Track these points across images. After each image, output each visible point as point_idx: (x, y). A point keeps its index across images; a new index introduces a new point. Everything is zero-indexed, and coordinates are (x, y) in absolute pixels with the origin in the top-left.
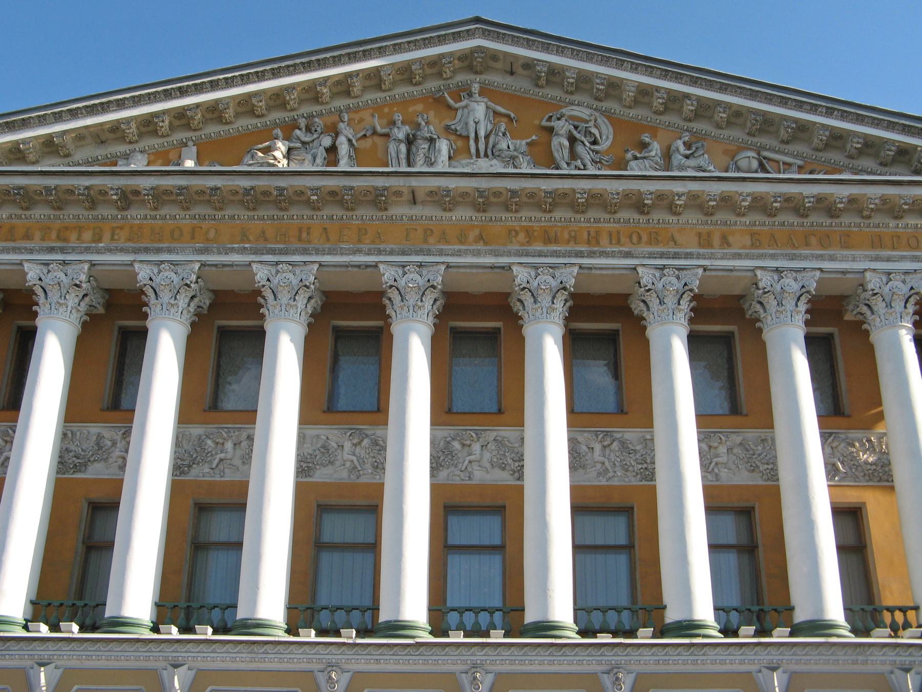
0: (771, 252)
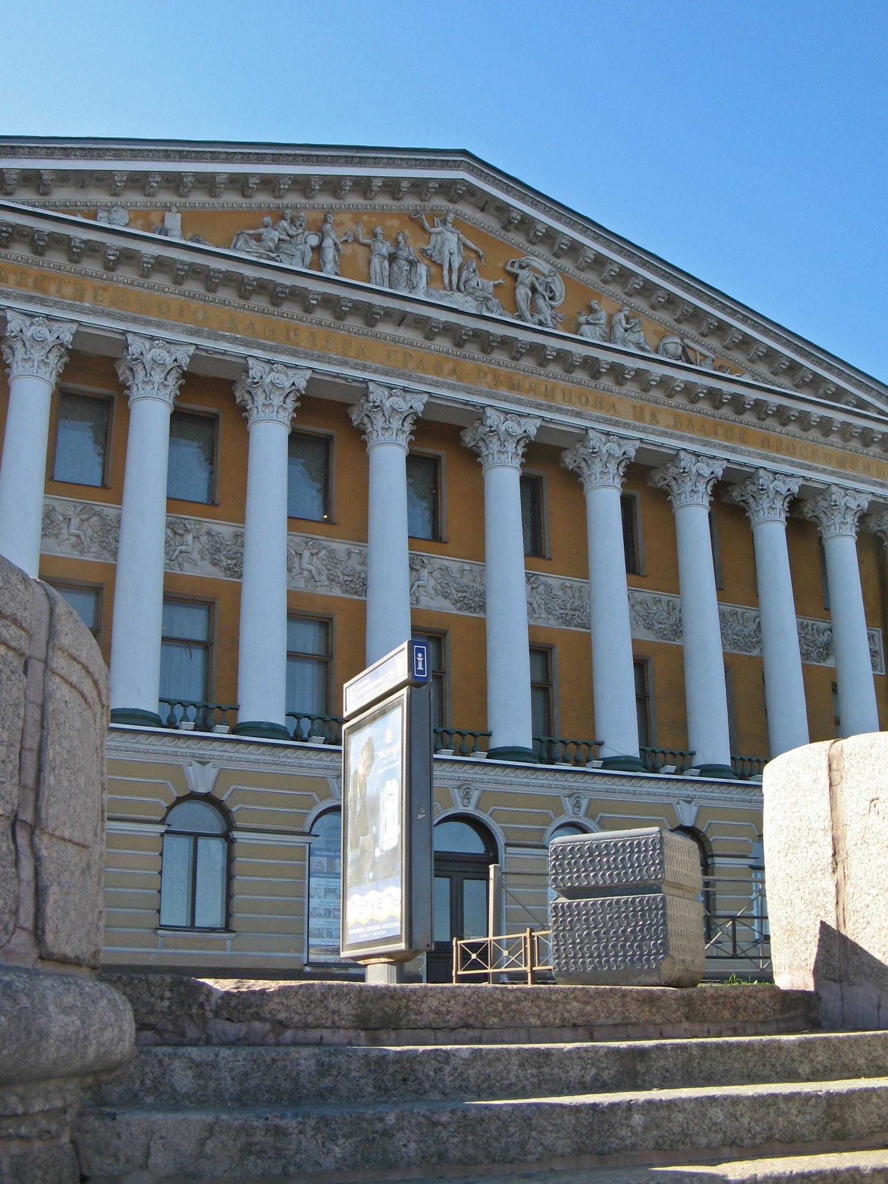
0: (690, 435)
